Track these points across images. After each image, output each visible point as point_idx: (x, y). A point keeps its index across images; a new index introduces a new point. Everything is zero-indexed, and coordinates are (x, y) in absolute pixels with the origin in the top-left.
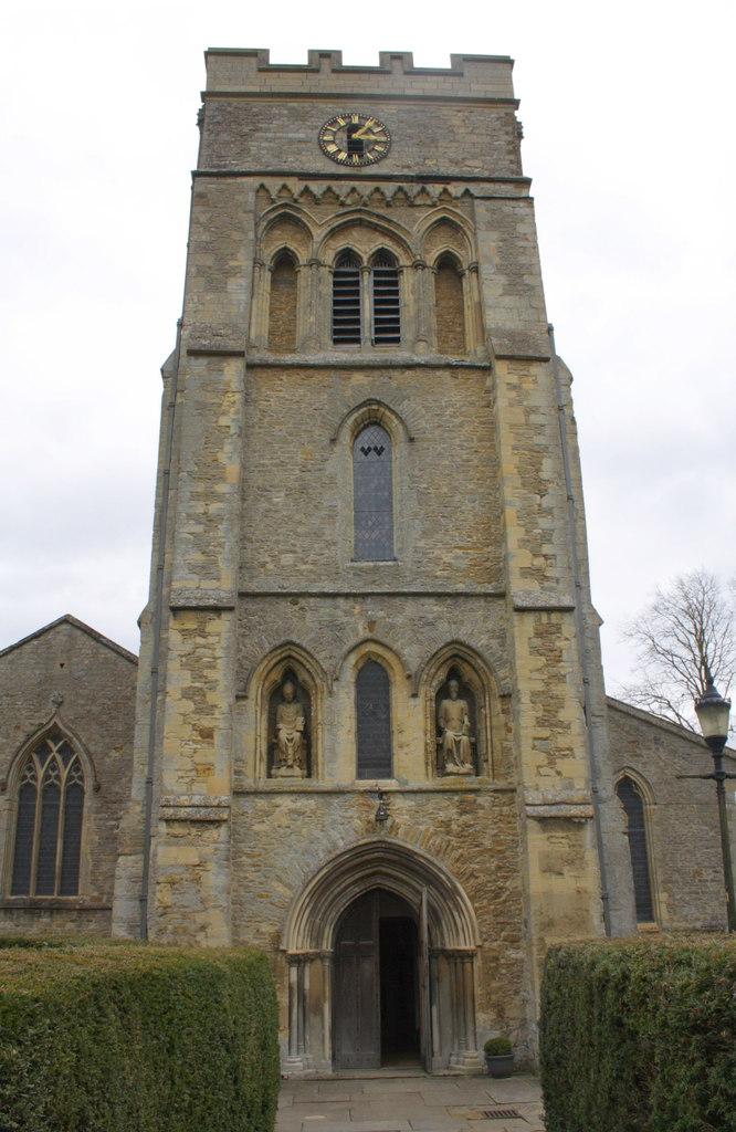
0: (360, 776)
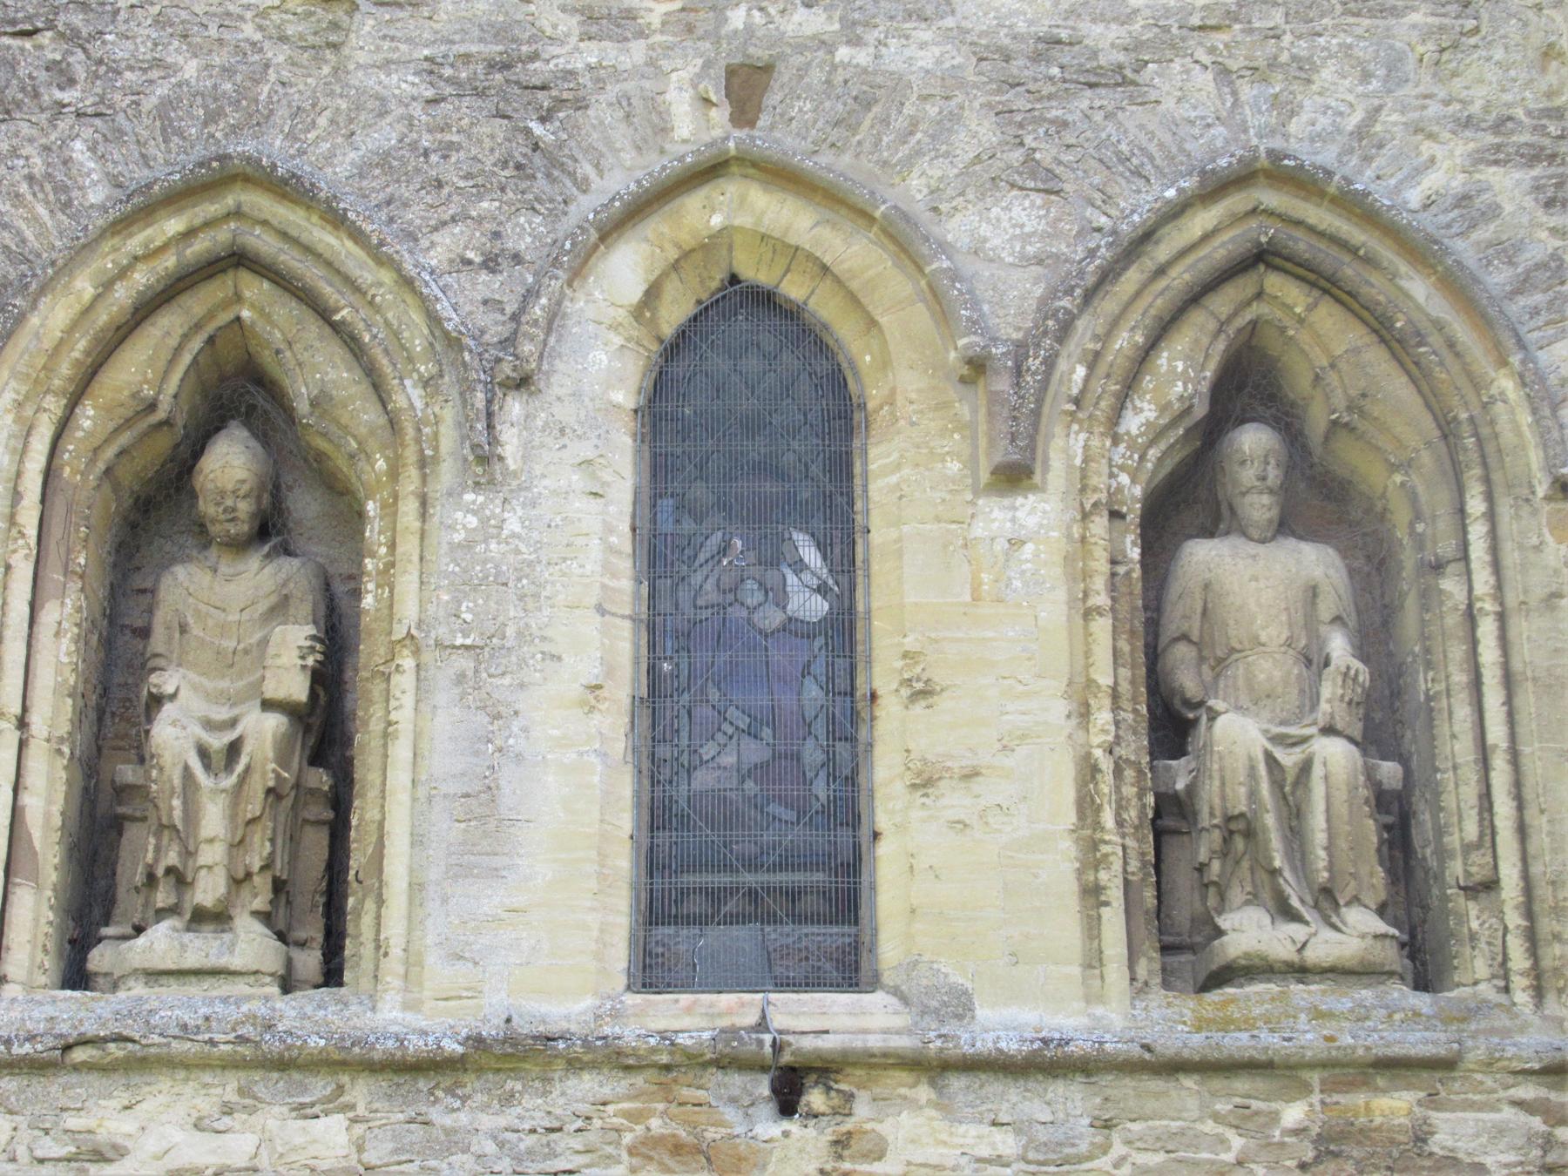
0: (651, 972)
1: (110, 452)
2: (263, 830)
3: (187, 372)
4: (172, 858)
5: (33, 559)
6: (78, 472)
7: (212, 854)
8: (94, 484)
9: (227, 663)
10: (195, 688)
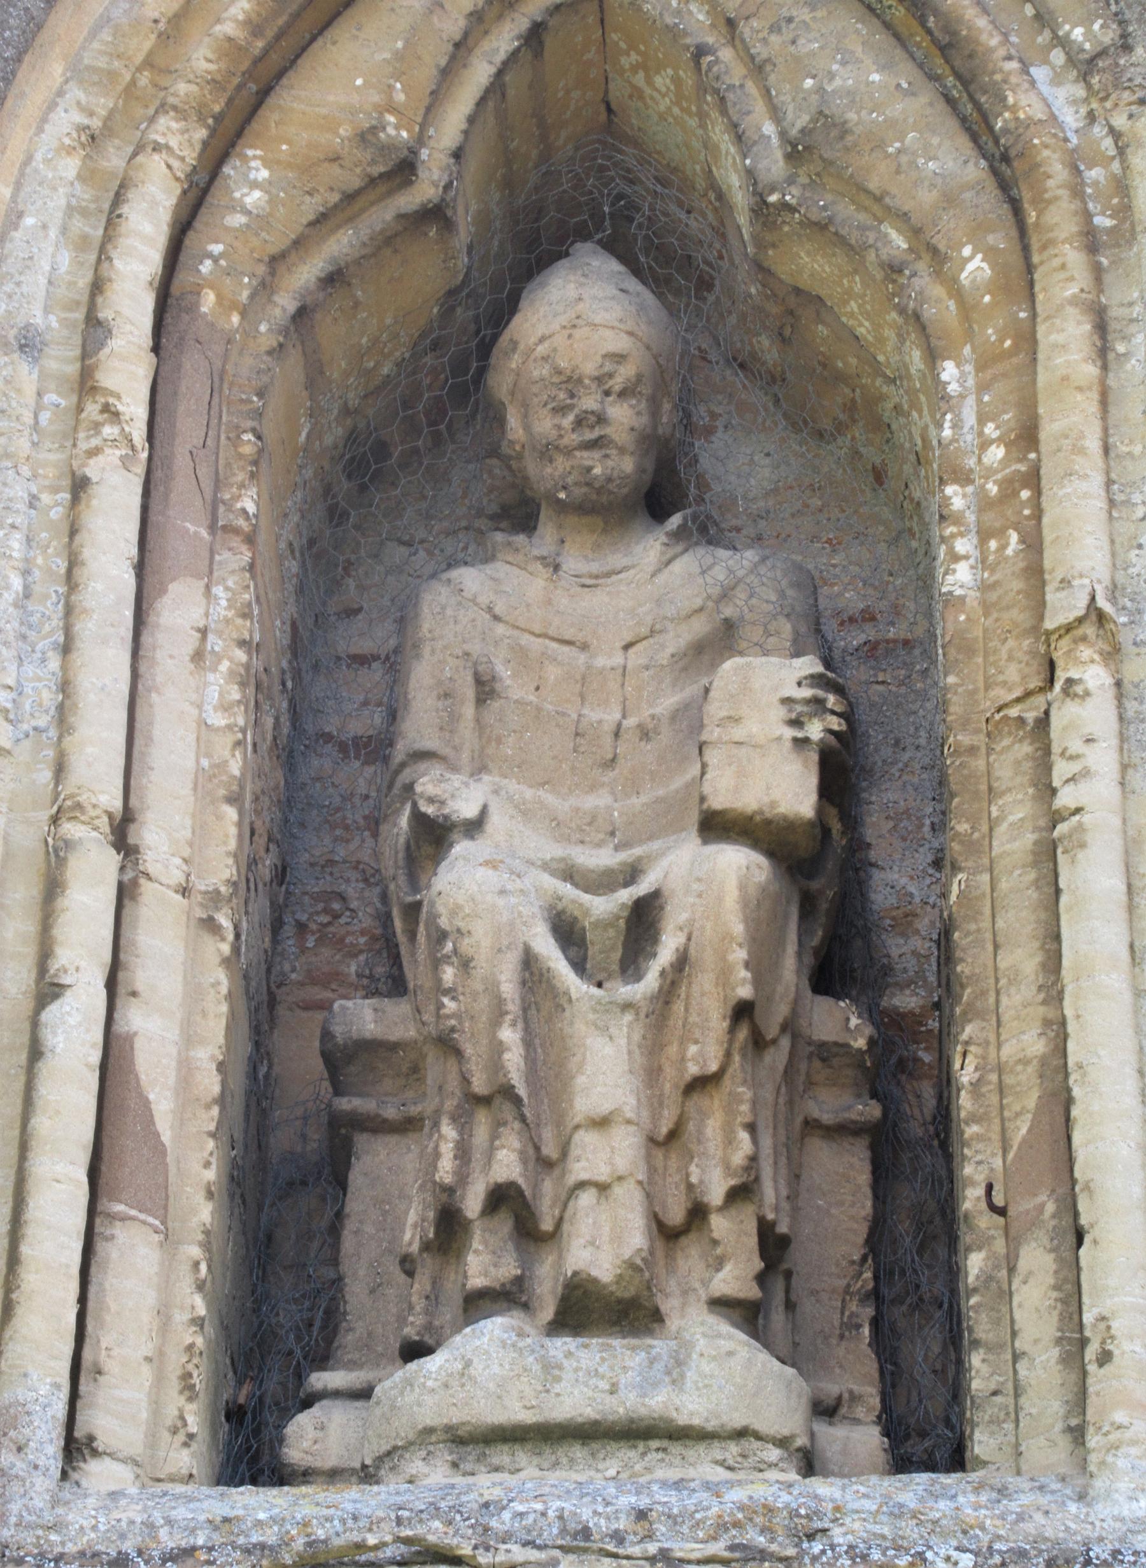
1: (306, 273)
2: (730, 1111)
3: (481, 102)
4: (507, 1164)
5: (140, 469)
6: (234, 306)
7: (608, 1156)
8: (273, 341)
9: (600, 756)
10: (525, 812)
